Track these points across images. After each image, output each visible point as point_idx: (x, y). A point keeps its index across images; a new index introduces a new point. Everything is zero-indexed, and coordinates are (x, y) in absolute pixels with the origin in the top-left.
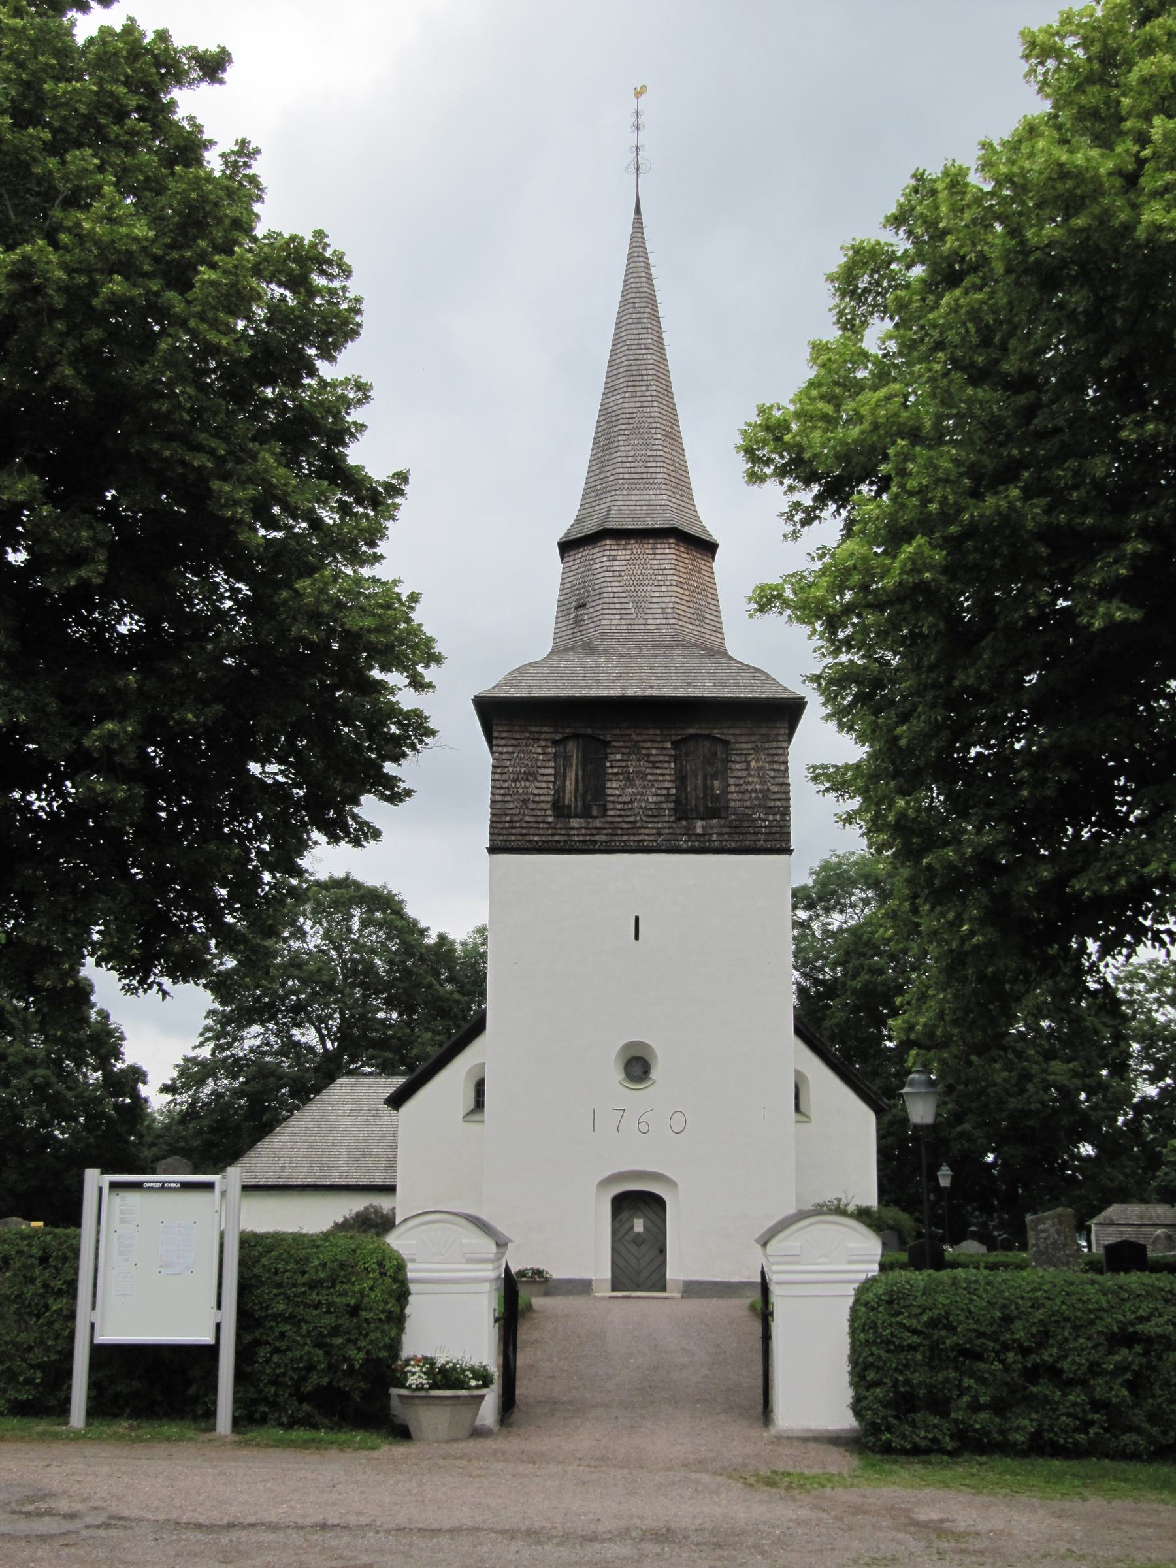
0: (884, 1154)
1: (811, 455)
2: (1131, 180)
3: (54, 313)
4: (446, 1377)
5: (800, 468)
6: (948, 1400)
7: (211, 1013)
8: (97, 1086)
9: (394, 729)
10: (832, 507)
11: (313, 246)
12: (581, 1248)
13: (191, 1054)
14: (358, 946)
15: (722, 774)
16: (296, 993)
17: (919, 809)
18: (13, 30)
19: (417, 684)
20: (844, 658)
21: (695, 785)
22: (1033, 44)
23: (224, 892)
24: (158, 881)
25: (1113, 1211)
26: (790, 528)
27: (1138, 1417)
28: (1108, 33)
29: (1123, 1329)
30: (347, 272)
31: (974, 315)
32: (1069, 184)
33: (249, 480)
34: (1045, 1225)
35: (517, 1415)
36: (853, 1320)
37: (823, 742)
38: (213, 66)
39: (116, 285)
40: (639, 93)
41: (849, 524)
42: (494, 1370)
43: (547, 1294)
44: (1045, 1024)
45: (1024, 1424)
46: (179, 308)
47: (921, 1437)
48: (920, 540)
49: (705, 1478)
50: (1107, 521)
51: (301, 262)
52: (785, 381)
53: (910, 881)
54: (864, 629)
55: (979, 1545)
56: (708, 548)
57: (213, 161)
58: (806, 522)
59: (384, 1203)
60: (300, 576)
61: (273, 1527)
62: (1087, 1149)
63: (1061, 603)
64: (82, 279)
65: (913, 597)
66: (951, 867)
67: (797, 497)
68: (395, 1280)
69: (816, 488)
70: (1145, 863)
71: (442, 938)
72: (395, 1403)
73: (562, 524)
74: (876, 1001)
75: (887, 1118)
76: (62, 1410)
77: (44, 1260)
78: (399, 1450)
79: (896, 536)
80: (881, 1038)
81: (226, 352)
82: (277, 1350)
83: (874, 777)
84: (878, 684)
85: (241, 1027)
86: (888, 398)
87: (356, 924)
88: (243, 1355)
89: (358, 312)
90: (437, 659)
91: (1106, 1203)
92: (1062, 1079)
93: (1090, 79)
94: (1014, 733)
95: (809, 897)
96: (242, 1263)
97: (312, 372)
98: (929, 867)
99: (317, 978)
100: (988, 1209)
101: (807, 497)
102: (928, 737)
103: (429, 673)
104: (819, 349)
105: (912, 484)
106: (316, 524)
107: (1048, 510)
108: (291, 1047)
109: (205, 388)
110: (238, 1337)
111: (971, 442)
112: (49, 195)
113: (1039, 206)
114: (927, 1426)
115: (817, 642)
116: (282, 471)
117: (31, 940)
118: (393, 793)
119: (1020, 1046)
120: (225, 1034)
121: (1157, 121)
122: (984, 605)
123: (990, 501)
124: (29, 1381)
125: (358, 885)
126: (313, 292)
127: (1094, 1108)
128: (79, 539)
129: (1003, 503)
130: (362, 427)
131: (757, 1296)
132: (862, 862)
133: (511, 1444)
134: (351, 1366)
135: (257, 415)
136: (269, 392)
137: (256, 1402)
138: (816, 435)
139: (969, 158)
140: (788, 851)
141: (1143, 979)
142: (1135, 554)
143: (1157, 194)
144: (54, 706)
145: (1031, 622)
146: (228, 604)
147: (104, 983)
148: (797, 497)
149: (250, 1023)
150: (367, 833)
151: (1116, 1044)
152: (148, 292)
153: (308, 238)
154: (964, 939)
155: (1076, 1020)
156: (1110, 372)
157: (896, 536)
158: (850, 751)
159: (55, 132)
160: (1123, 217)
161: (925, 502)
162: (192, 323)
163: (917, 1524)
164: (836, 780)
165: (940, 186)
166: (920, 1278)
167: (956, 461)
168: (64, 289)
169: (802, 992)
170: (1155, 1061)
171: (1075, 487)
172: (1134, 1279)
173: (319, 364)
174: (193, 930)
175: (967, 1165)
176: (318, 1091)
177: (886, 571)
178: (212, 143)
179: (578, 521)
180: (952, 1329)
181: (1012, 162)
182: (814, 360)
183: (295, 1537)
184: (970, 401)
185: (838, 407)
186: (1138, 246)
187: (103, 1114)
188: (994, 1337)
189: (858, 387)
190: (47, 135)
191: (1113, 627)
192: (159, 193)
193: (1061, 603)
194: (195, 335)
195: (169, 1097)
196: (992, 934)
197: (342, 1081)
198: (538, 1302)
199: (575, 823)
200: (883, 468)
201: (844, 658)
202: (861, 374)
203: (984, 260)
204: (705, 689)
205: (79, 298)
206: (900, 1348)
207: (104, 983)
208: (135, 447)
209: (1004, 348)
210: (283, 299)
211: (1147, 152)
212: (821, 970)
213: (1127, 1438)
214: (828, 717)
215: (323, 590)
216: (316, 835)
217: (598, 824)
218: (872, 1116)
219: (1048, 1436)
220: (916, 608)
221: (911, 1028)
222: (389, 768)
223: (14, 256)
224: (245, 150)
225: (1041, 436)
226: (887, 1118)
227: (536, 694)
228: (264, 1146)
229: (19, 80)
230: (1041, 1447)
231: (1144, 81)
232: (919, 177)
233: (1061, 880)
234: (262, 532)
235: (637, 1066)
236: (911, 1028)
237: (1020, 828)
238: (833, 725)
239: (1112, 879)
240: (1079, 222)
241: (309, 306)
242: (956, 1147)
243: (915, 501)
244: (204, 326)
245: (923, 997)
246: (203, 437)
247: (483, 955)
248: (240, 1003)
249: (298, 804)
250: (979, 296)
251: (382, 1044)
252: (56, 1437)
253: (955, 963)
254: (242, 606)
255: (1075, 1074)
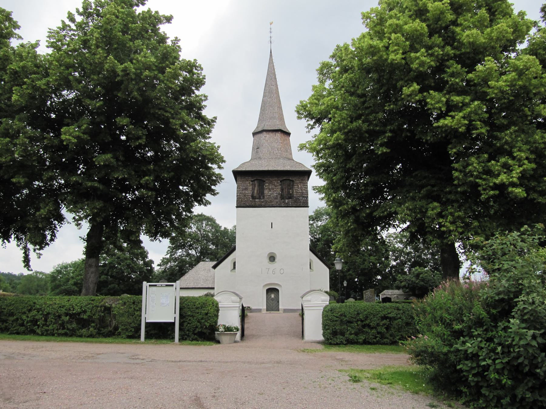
0: (331, 279)
1: (313, 113)
2: (387, 48)
3: (132, 80)
4: (228, 329)
5: (310, 115)
6: (344, 332)
7: (169, 247)
8: (142, 265)
9: (214, 178)
10: (318, 125)
11: (194, 63)
12: (259, 301)
13: (165, 257)
14: (205, 231)
15: (292, 188)
16: (190, 242)
17: (338, 197)
18: (122, 12)
19: (220, 167)
20: (321, 161)
21: (286, 191)
22: (364, 16)
23: (174, 217)
24: (158, 214)
25: (385, 292)
26: (308, 130)
27: (388, 335)
28: (382, 14)
29: (385, 316)
30: (202, 69)
31: (351, 80)
32: (373, 49)
33: (179, 119)
34: (368, 293)
35: (245, 338)
36: (323, 315)
37: (316, 181)
38: (169, 19)
39: (147, 73)
40: (271, 24)
41: (322, 129)
42: (240, 327)
43: (251, 312)
44: (369, 247)
45: (362, 338)
46: (162, 78)
47: (338, 341)
48: (338, 133)
49: (289, 350)
50: (382, 128)
51: (191, 67)
52: (306, 95)
53: (336, 213)
54: (325, 154)
55: (351, 363)
56: (288, 134)
57: (169, 42)
58: (311, 129)
59: (212, 292)
60: (192, 142)
61: (190, 362)
62: (379, 277)
63: (372, 147)
64: (139, 71)
65: (337, 146)
66: (346, 210)
67: (309, 122)
68: (216, 307)
69: (314, 120)
70: (390, 208)
71: (225, 228)
72: (216, 335)
73: (253, 128)
74: (328, 243)
75: (332, 270)
76: (139, 337)
77: (134, 303)
78: (218, 345)
79: (333, 132)
80: (330, 251)
81: (173, 88)
82: (189, 323)
83: (328, 189)
84: (328, 167)
85: (177, 250)
86: (331, 99)
87: (204, 225)
88: (181, 324)
89: (205, 79)
90: (224, 161)
91: (383, 290)
92: (373, 261)
93: (378, 24)
94: (361, 179)
95: (313, 218)
96: (180, 303)
97: (194, 93)
98: (341, 210)
99: (196, 239)
100: (356, 292)
101: (312, 122)
102: (341, 179)
103: (222, 165)
104: (314, 87)
105: (336, 120)
106: (195, 129)
107: (368, 126)
108: (188, 255)
109: (168, 97)
110: (180, 320)
111: (350, 110)
112: (130, 51)
113: (366, 54)
114: (340, 338)
115: (314, 157)
116: (187, 117)
117: (129, 229)
118: (214, 193)
119: (363, 253)
120: (173, 252)
121: (393, 35)
122: (354, 148)
123: (354, 124)
124: (131, 331)
125: (205, 216)
126: (193, 74)
127: (381, 267)
128: (139, 133)
129: (358, 124)
130: (206, 106)
131: (301, 312)
132: (326, 209)
133: (243, 344)
134: (206, 327)
135: (181, 103)
136: (183, 98)
137: (184, 335)
138: (314, 108)
139: (349, 42)
140: (308, 207)
141: (393, 237)
142: (388, 136)
143: (393, 52)
144: (133, 173)
145: (364, 152)
146: (174, 148)
147: (144, 238)
148: (309, 122)
149: (179, 249)
150: (207, 203)
151: (386, 252)
152: (155, 74)
153: (193, 61)
154: (349, 227)
155: (376, 247)
156: (383, 93)
157: (333, 132)
158: (322, 183)
159: (132, 36)
160: (385, 57)
161: (339, 124)
162: (165, 82)
163: (337, 359)
164: (319, 190)
165: (342, 49)
166: (338, 305)
167: (346, 114)
168: (135, 74)
169: (311, 240)
170: (395, 256)
171: (374, 120)
172: (387, 304)
173: (195, 91)
174: (167, 226)
175: (351, 281)
176: (195, 265)
177: (330, 140)
178: (169, 38)
179: (257, 127)
180: (345, 316)
181: (359, 44)
182: (313, 90)
183: (194, 363)
184: (350, 100)
185: (319, 101)
186: (389, 64)
187: (143, 271)
188: (355, 318)
189: (323, 97)
190: (130, 37)
191: (383, 153)
192: (156, 50)
193: (372, 147)
194: (166, 84)
195: (159, 267)
196: (355, 225)
197: (201, 263)
198: (249, 314)
199: (257, 200)
200: (330, 116)
201: (321, 161)
202: (324, 93)
203: (353, 66)
204: (288, 168)
205: (138, 76)
206: (334, 321)
207: (144, 238)
208: (152, 111)
209: (358, 87)
210: (186, 75)
211: (390, 42)
212: (316, 235)
213: (385, 340)
214: (317, 175)
215: (197, 145)
216: (196, 203)
217: (262, 200)
218: (328, 270)
219: (367, 340)
220: (337, 149)
221: (337, 248)
222: (213, 187)
223: (123, 66)
224: (177, 40)
225: (367, 108)
226: (332, 270)
227: (247, 169)
228: (183, 278)
229: (123, 24)
230: (366, 342)
231: (390, 25)
232: (338, 46)
233: (371, 213)
234: (182, 131)
235: (272, 258)
236: (337, 248)
237: (362, 200)
238: (318, 177)
239: (383, 212)
240: (375, 58)
241: (193, 78)
242: (348, 277)
243: (337, 124)
244: (168, 82)
245: (339, 241)
246: (168, 109)
247: (235, 233)
248: (176, 245)
249: (191, 196)
250: (352, 75)
251: (211, 254)
252: (138, 343)
253: (347, 233)
254: (178, 149)
255: (376, 259)
